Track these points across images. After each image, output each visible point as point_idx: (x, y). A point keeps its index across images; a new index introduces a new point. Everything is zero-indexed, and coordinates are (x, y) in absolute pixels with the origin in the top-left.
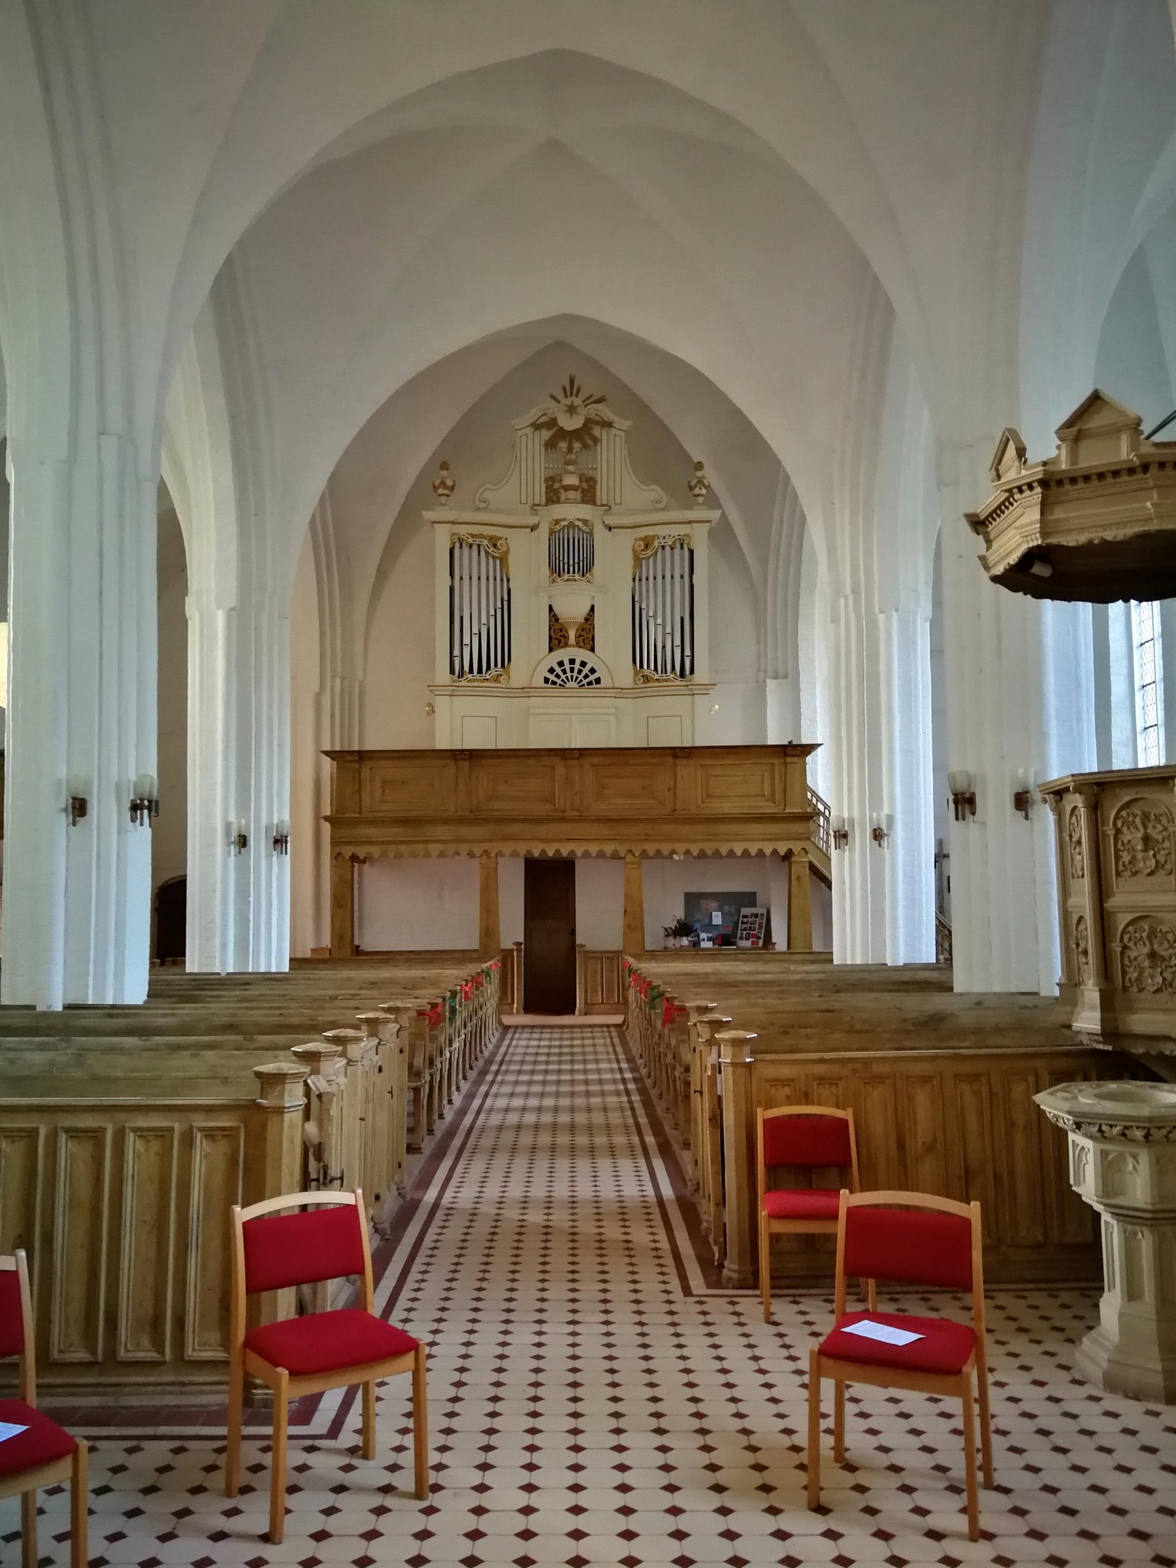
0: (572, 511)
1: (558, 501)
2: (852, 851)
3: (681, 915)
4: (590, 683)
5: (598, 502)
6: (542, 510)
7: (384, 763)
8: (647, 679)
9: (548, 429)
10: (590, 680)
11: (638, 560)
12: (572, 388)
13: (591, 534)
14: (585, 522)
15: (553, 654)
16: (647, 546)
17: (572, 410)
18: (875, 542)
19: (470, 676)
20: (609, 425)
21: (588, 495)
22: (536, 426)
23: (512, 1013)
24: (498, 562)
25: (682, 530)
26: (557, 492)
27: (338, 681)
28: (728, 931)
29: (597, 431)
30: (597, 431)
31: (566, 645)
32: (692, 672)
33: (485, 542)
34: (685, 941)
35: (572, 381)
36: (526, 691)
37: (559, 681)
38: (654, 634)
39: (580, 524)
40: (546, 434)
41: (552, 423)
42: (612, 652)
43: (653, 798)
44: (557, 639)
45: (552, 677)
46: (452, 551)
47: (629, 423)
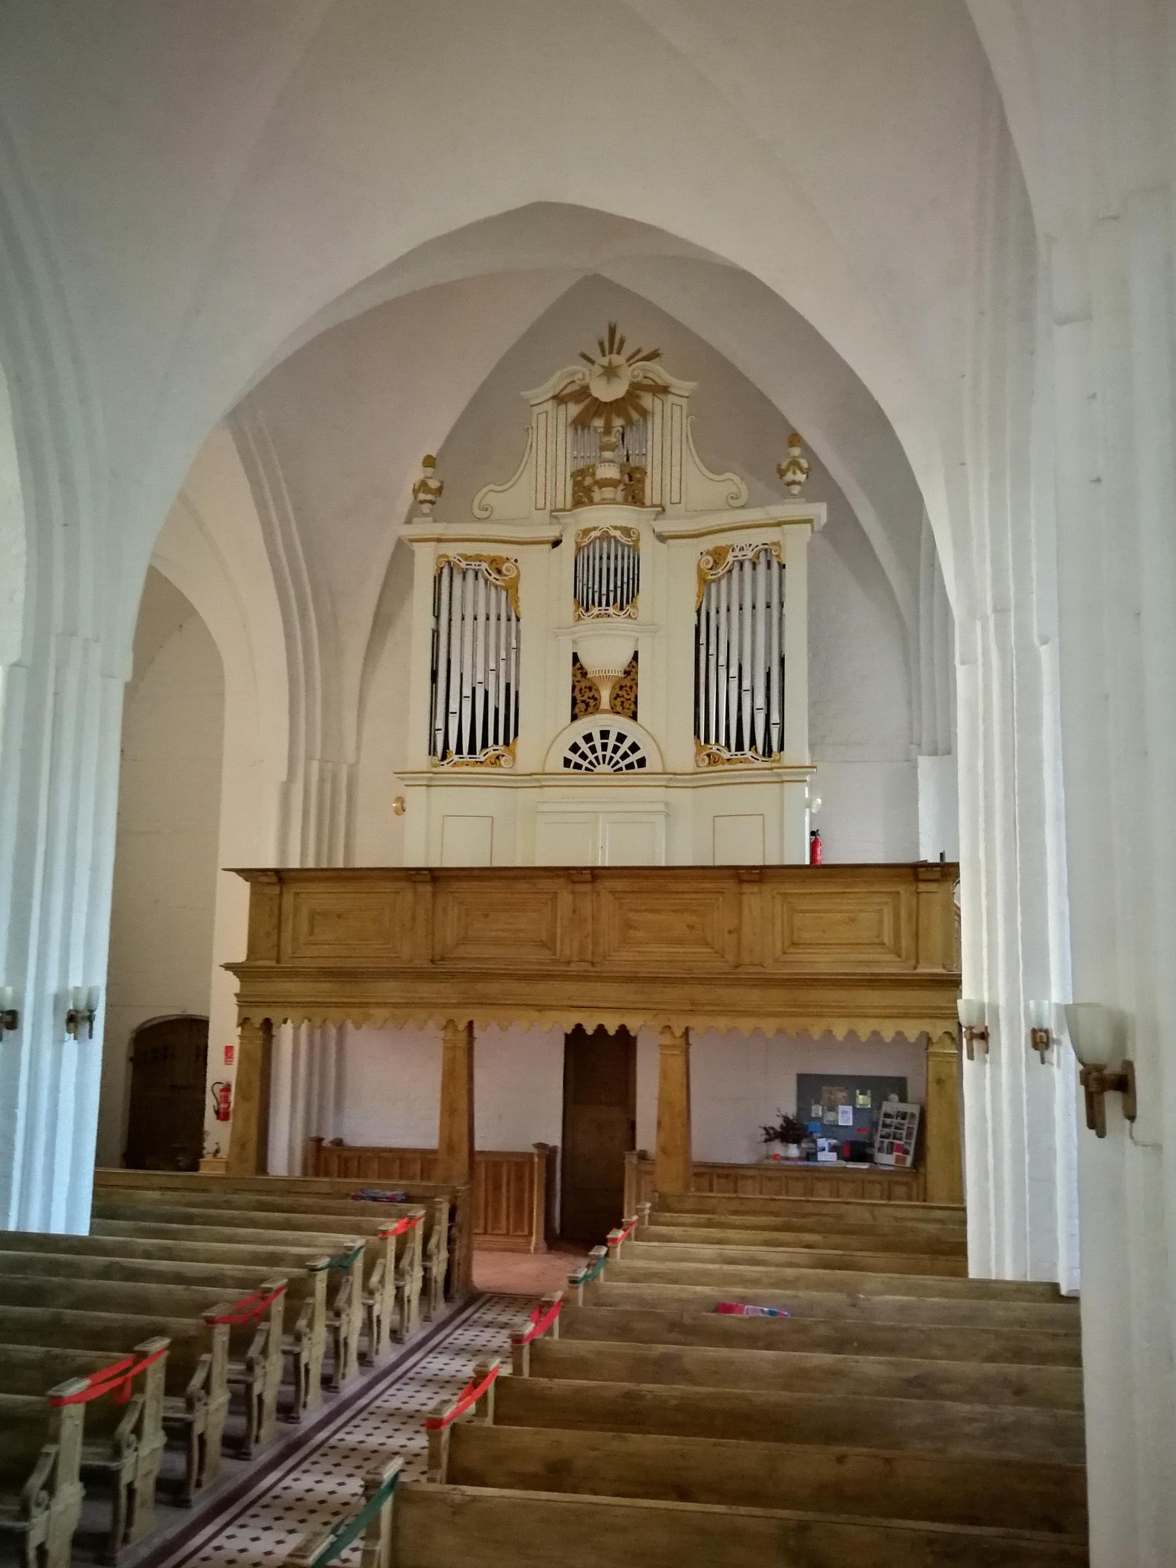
0: (609, 516)
1: (591, 502)
2: (996, 1064)
3: (790, 1109)
4: (630, 766)
5: (648, 502)
6: (567, 519)
7: (313, 887)
8: (713, 759)
9: (578, 402)
10: (630, 760)
11: (704, 582)
12: (612, 342)
13: (635, 548)
14: (626, 531)
15: (577, 723)
16: (716, 564)
17: (610, 372)
18: (1033, 522)
19: (456, 758)
20: (665, 390)
21: (632, 487)
22: (560, 399)
23: (527, 1252)
24: (504, 594)
25: (769, 536)
26: (588, 490)
27: (315, 765)
28: (861, 1137)
29: (647, 400)
30: (647, 400)
31: (597, 709)
32: (781, 748)
33: (485, 566)
34: (793, 1151)
35: (612, 331)
36: (538, 779)
37: (585, 764)
38: (723, 689)
39: (618, 534)
40: (574, 410)
41: (583, 393)
42: (664, 720)
43: (707, 944)
44: (583, 701)
45: (575, 758)
46: (438, 580)
47: (692, 385)
